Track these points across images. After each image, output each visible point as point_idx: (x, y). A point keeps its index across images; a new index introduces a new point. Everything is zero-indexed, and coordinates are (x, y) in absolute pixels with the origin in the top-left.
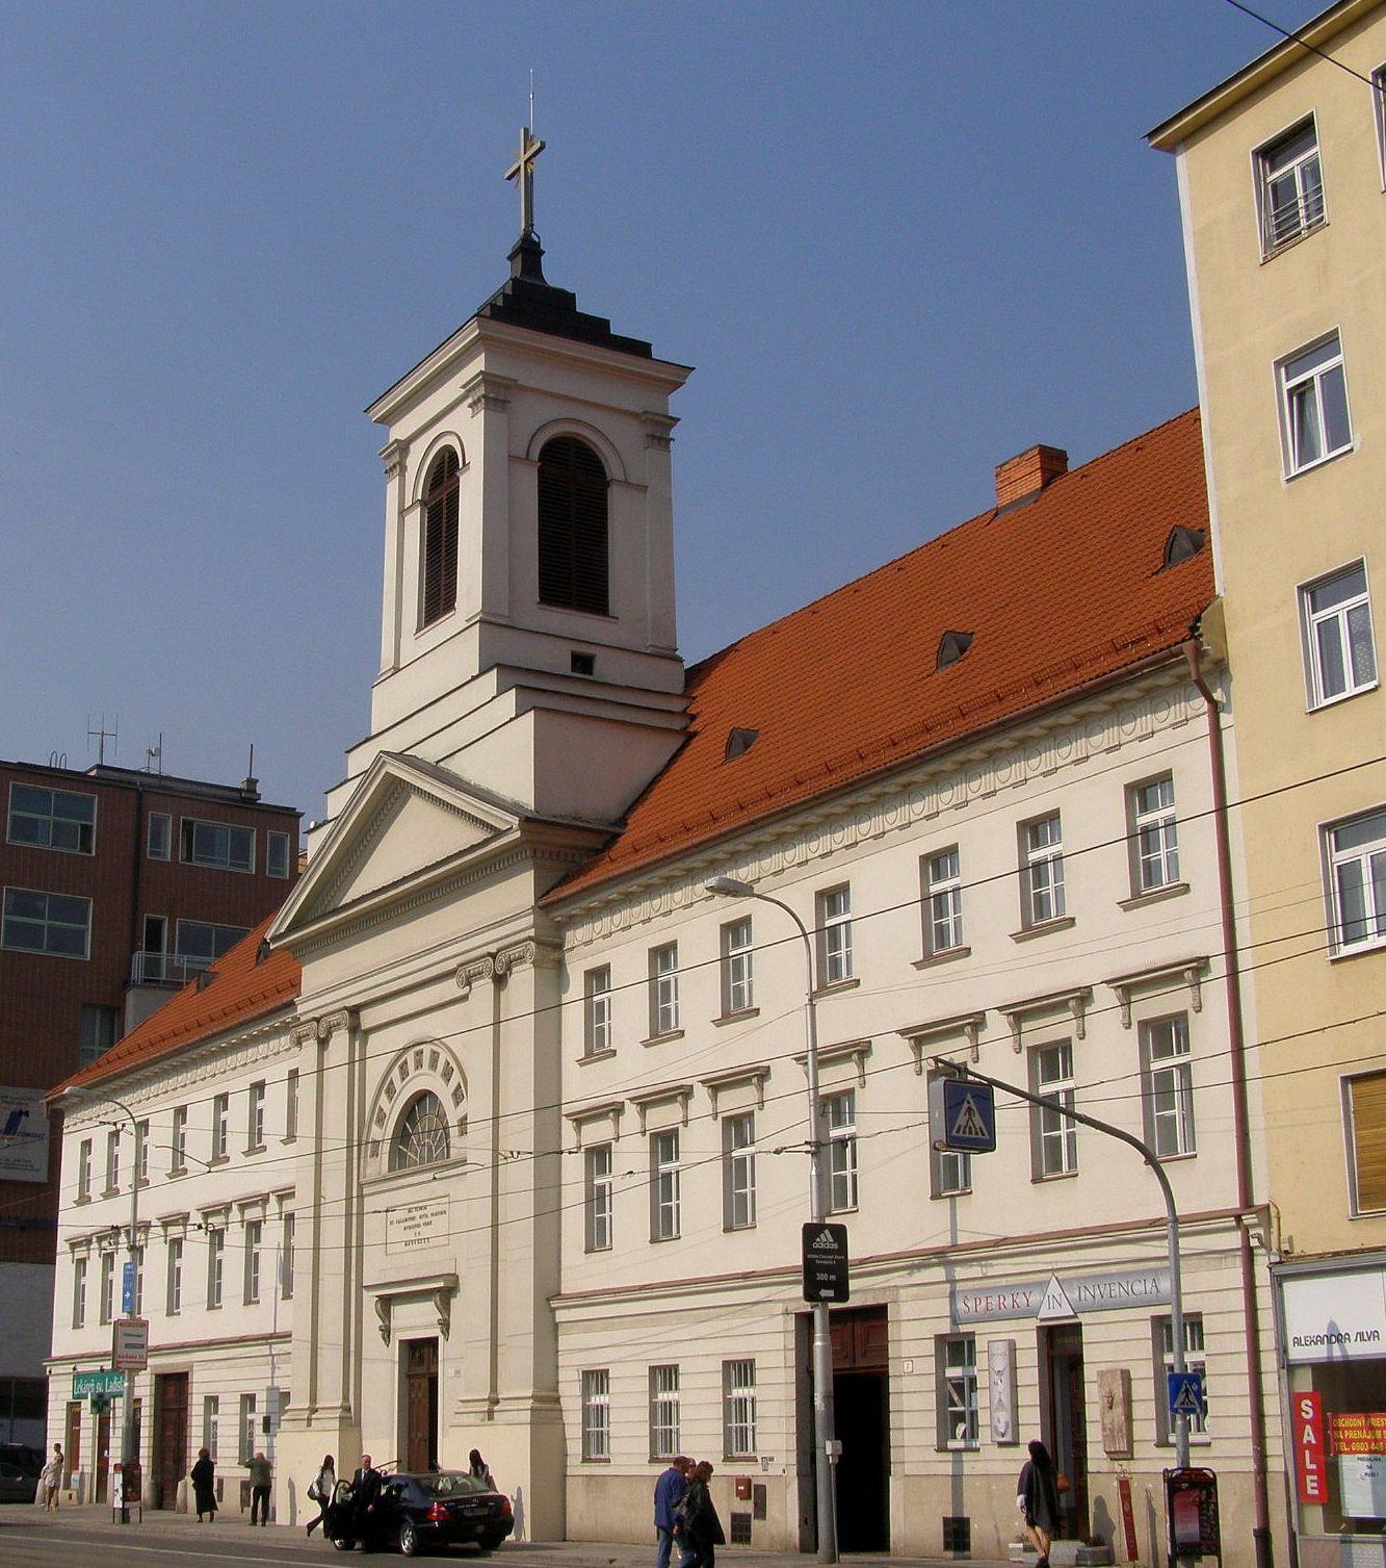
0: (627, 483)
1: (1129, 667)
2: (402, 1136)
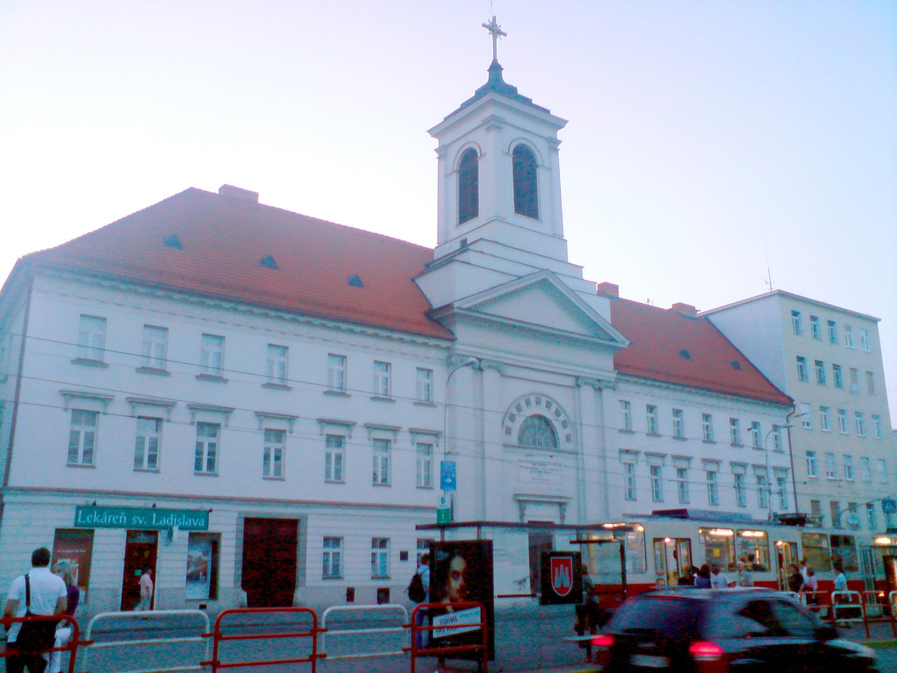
0: (543, 167)
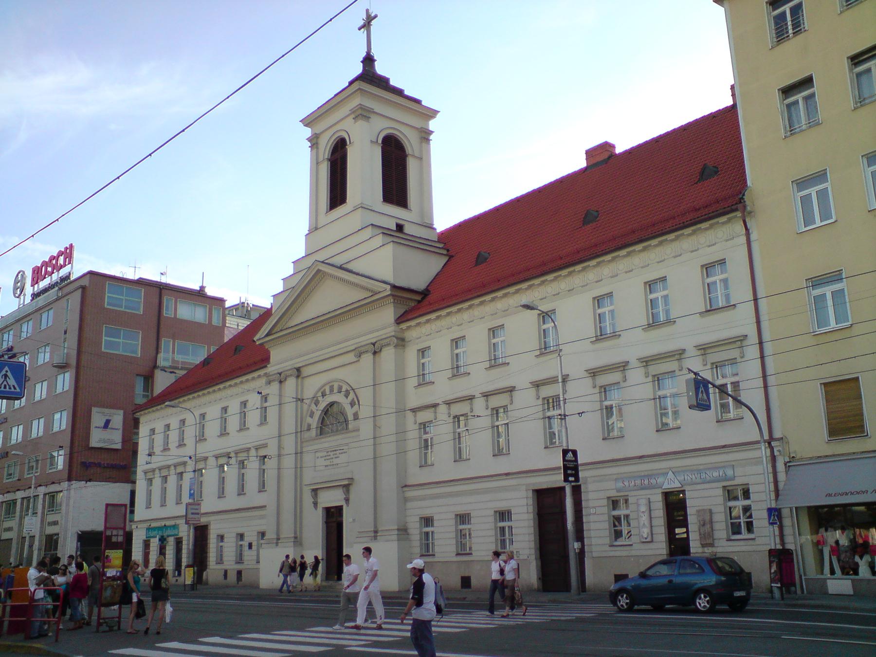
0: (413, 156)
1: (710, 215)
2: (322, 421)
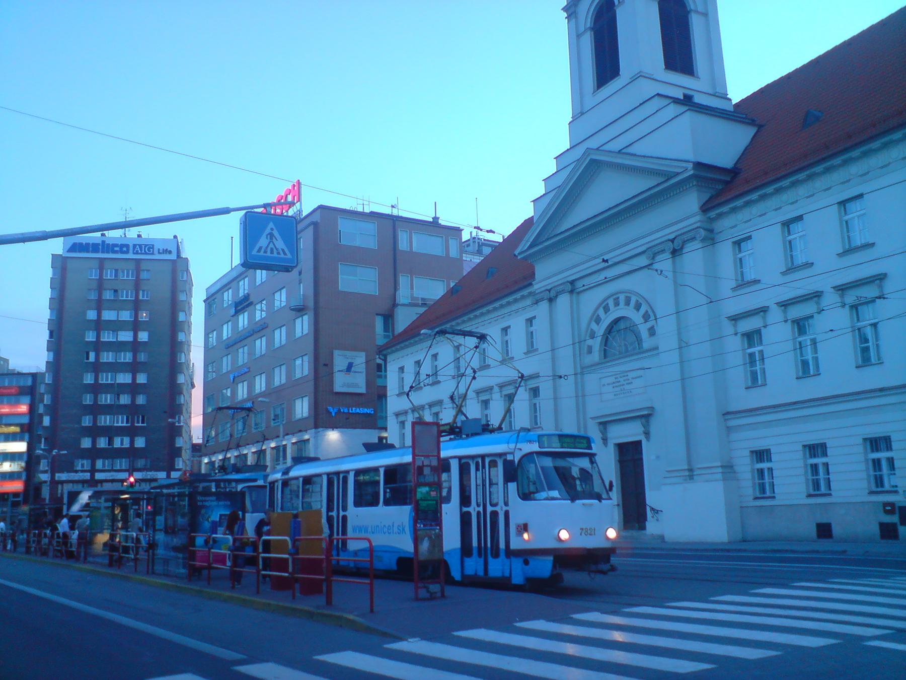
0: (697, 12)
2: (606, 341)
